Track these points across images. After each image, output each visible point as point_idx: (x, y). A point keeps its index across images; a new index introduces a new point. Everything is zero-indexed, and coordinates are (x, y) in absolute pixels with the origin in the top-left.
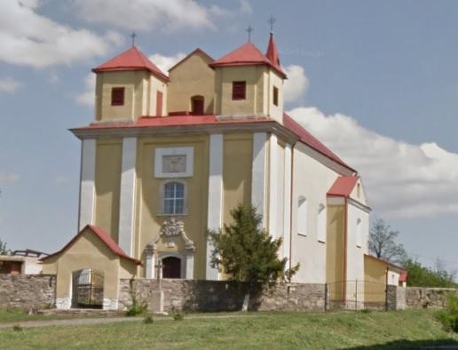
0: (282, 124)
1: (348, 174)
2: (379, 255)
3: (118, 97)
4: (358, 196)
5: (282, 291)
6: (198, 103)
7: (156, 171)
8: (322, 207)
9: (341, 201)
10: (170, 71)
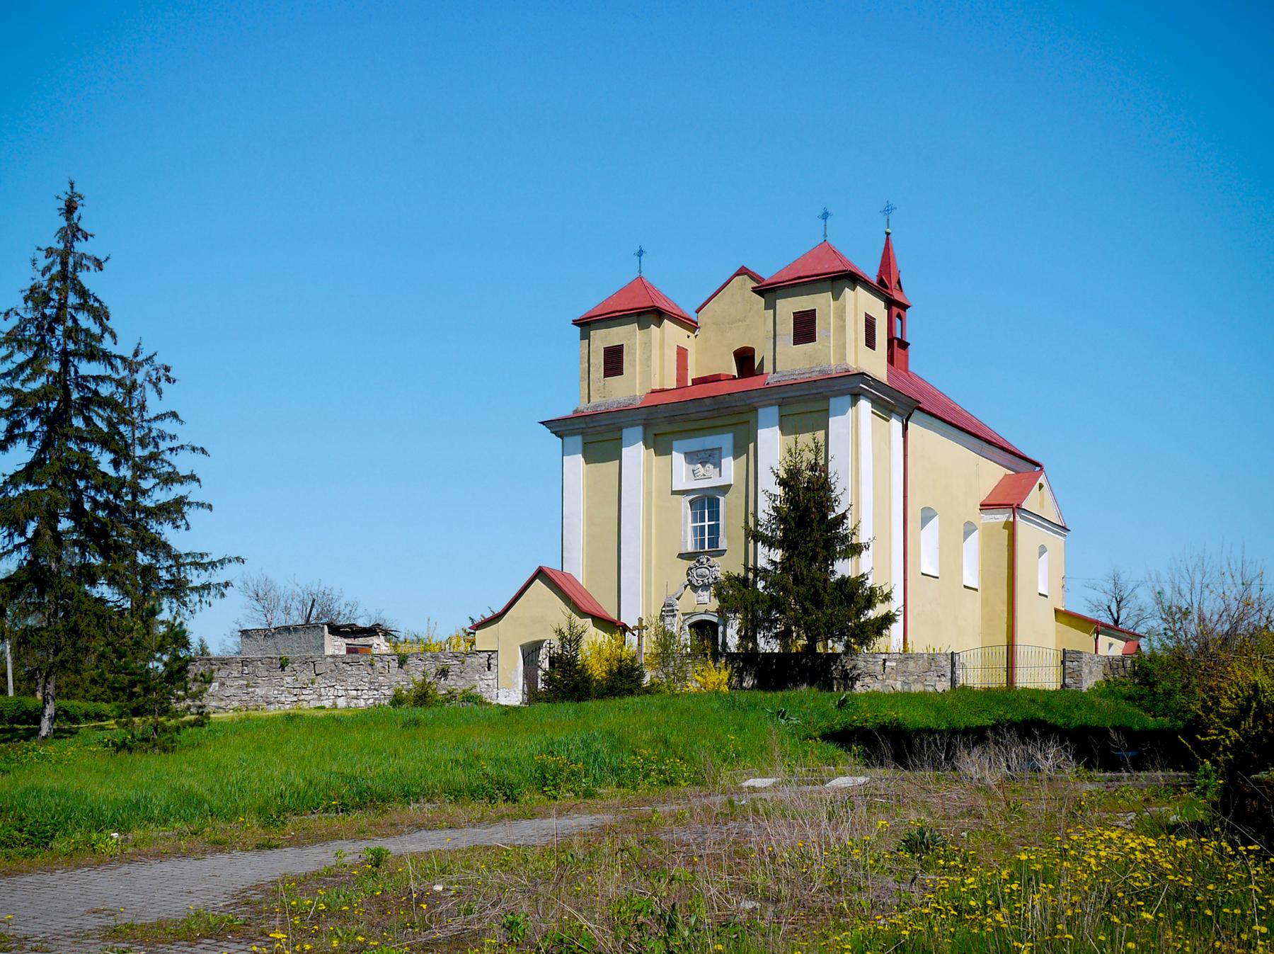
0: (885, 380)
1: (1025, 466)
2: (1116, 622)
3: (614, 361)
4: (1042, 506)
5: (871, 667)
6: (745, 358)
7: (965, 573)
8: (969, 529)
9: (1002, 517)
10: (698, 312)
